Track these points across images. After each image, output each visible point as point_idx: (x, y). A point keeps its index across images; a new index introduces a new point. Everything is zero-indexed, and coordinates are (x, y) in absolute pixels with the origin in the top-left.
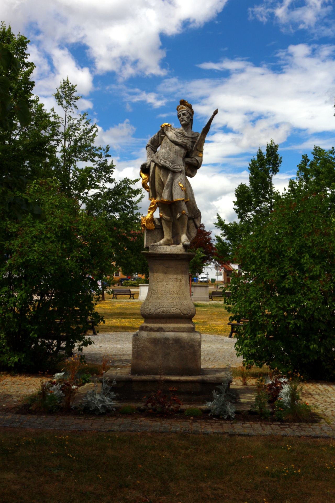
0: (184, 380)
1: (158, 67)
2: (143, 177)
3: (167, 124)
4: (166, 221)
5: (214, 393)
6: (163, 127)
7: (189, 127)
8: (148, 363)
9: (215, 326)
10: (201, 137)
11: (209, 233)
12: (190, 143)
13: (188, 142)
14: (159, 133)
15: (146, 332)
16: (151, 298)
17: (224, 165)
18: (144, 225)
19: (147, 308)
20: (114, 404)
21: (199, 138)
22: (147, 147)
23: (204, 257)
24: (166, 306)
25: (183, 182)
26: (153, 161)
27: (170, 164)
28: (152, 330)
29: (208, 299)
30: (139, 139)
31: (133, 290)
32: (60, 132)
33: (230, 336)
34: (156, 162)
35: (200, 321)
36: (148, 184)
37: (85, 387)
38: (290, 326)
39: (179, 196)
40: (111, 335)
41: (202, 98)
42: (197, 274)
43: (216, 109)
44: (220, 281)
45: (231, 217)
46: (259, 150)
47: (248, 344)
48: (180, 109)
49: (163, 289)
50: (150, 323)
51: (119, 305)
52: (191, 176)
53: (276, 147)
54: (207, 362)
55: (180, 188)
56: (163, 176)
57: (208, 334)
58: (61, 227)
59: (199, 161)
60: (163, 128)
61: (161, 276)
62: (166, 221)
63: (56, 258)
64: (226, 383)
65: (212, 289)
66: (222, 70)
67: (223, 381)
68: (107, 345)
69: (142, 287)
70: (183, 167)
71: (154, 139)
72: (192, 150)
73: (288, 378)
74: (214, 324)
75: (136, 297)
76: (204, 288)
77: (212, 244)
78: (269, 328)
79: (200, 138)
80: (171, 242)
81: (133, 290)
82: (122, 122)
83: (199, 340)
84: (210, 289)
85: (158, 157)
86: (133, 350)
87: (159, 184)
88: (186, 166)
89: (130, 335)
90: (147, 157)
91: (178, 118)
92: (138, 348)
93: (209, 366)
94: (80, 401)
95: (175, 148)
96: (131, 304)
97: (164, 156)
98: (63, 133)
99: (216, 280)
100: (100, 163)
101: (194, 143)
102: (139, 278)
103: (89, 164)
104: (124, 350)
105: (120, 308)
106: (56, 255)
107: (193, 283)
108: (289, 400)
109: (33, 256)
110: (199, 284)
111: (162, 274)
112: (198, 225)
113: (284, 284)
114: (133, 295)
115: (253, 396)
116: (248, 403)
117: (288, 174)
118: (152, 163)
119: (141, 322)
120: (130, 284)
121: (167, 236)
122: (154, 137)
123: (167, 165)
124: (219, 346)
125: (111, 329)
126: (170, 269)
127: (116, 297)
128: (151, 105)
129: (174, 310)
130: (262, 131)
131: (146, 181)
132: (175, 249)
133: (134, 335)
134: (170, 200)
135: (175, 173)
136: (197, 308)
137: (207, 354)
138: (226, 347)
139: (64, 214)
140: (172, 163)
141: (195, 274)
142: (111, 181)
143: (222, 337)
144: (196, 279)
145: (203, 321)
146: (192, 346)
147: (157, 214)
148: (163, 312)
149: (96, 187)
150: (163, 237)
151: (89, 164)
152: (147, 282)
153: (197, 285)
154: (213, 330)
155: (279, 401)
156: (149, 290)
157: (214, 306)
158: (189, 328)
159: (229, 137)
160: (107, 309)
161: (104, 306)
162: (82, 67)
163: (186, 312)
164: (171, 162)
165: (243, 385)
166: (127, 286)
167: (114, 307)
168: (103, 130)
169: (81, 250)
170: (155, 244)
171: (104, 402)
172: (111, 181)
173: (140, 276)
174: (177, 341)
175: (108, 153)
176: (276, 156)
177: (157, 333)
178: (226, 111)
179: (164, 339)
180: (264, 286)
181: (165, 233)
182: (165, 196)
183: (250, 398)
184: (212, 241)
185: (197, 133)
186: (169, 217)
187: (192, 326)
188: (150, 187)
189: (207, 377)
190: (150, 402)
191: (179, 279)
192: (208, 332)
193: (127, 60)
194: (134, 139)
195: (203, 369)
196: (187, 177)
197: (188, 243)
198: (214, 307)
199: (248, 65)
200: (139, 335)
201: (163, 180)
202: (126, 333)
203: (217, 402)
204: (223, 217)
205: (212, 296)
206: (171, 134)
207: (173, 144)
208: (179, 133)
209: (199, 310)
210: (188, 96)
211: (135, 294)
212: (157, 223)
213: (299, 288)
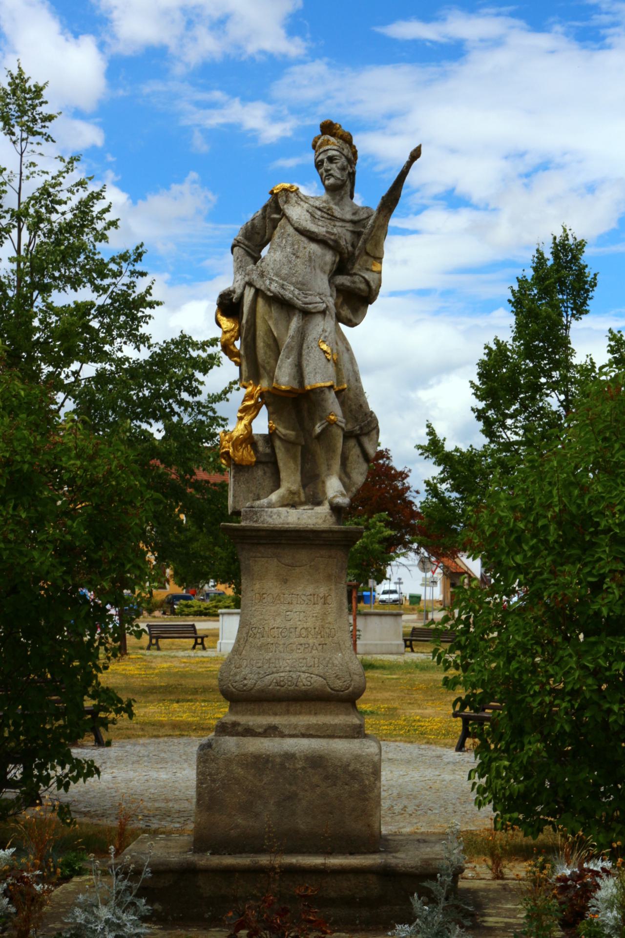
0: (334, 865)
1: (282, 32)
2: (224, 326)
3: (287, 185)
4: (285, 441)
5: (416, 902)
6: (277, 194)
7: (345, 193)
9: (419, 721)
10: (377, 218)
11: (403, 475)
12: (348, 236)
13: (343, 233)
16: (247, 648)
17: (447, 293)
18: (227, 453)
19: (235, 675)
20: (148, 931)
21: (371, 222)
22: (233, 247)
23: (391, 537)
24: (288, 668)
26: (250, 284)
27: (297, 292)
28: (249, 732)
29: (402, 648)
30: (223, 226)
31: (202, 625)
32: (5, 208)
33: (460, 747)
34: (258, 286)
35: (379, 708)
36: (238, 344)
37: (69, 886)
39: (319, 377)
40: (144, 747)
41: (390, 116)
42: (372, 583)
43: (417, 145)
44: (433, 601)
45: (464, 434)
46: (538, 250)
48: (320, 147)
49: (279, 622)
51: (165, 665)
52: (351, 324)
53: (580, 246)
54: (397, 818)
55: (322, 356)
56: (276, 324)
57: (401, 741)
59: (372, 284)
60: (275, 196)
61: (272, 587)
62: (285, 441)
64: (448, 875)
65: (411, 620)
66: (443, 40)
67: (438, 870)
68: (131, 774)
69: (226, 618)
70: (330, 299)
71: (253, 226)
72: (353, 254)
73: (613, 857)
74: (417, 714)
75: (211, 644)
76: (388, 621)
77: (411, 503)
78: (559, 725)
79: (375, 222)
80: (299, 497)
81: (202, 625)
82: (180, 181)
83: (376, 758)
84: (408, 621)
85: (263, 272)
86: (198, 787)
87: (268, 346)
88: (337, 297)
89: (191, 746)
90: (235, 273)
91: (315, 170)
92: (213, 781)
93: (404, 827)
94: (58, 925)
95: (308, 249)
96: (197, 663)
97: (280, 269)
98: (13, 210)
99: (423, 598)
101: (357, 234)
102: (219, 594)
103: (85, 294)
104: (177, 785)
105: (169, 674)
107: (361, 605)
108: (616, 918)
110: (376, 608)
112: (372, 453)
113: (595, 607)
114: (202, 638)
115: (520, 910)
116: (508, 926)
117: (616, 315)
118: (247, 288)
119: (221, 712)
120: (196, 609)
121: (290, 481)
122: (253, 220)
123: (288, 295)
124: (430, 773)
125: (143, 730)
126: (298, 570)
127: (157, 643)
128: (252, 136)
129: (308, 680)
130: (550, 201)
131: (232, 336)
132: (309, 517)
133: (202, 747)
134: (296, 386)
135: (307, 314)
136: (370, 674)
137: (398, 794)
138: (447, 777)
139: (17, 428)
140: (299, 289)
141: (367, 583)
142: (143, 340)
143: (439, 750)
144: (369, 596)
145: (388, 708)
146: (355, 776)
147: (261, 425)
148: (278, 684)
149: (103, 356)
150: (277, 486)
151: (85, 294)
152: (237, 605)
153: (372, 610)
154: (415, 730)
155: (591, 923)
156: (242, 625)
157: (417, 666)
158: (349, 726)
159: (463, 219)
160: (132, 676)
161: (124, 670)
162: (76, 36)
163: (338, 684)
165: (494, 879)
166: (188, 615)
167: (151, 671)
168: (130, 201)
170: (258, 503)
171: (120, 927)
173: (221, 587)
174: (316, 761)
176: (581, 273)
177: (262, 740)
178: (453, 151)
179: (280, 756)
180: (544, 613)
181: (283, 475)
182: (284, 377)
183: (512, 913)
184: (410, 496)
185: (367, 208)
187: (356, 721)
188: (242, 352)
189: (396, 858)
190: (243, 928)
191: (321, 595)
192: (401, 735)
193: (198, 15)
194: (211, 225)
195: (386, 835)
196: (341, 325)
197: (344, 501)
198: (418, 671)
199: (512, 27)
200: (214, 745)
201: (276, 335)
202: (183, 740)
203: (424, 926)
204: (440, 433)
205: (411, 641)
206: (296, 212)
207: (303, 239)
208: (319, 209)
209: (378, 678)
210: (354, 111)
211: (207, 636)
212: (261, 449)
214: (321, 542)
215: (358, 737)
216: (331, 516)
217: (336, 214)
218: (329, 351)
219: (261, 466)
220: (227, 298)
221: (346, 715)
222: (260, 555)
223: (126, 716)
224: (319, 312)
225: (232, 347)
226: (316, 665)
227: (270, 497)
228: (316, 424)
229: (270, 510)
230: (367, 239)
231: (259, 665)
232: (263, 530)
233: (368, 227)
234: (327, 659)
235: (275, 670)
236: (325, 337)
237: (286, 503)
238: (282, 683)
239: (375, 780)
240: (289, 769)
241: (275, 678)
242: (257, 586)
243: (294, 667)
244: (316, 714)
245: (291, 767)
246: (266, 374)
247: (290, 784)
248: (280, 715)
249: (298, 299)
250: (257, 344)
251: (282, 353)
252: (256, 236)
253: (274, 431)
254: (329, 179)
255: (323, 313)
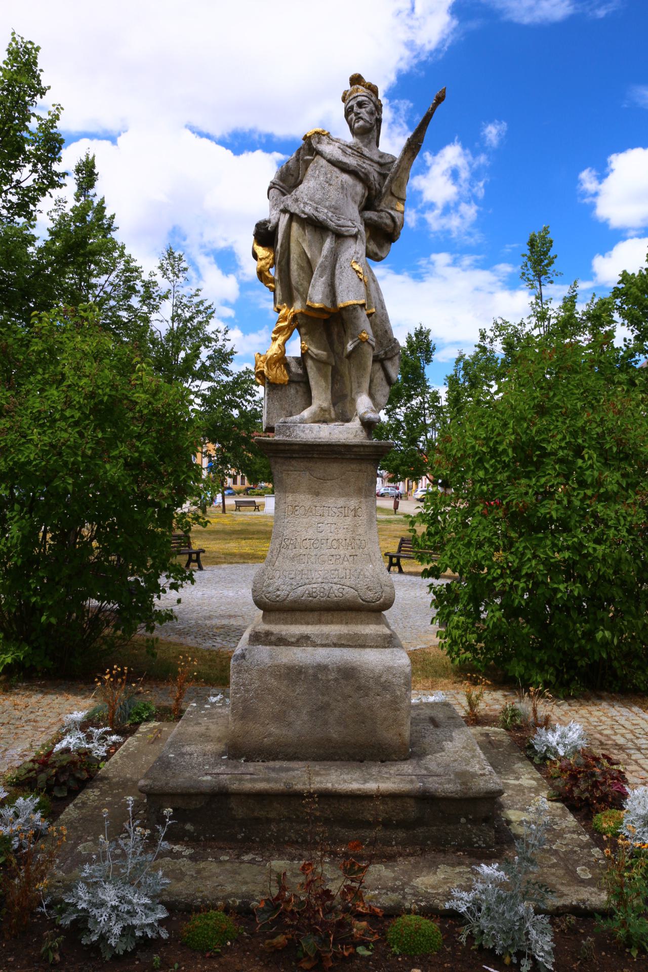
4: (317, 361)
8: (273, 729)
14: (298, 152)
15: (268, 647)
16: (280, 558)
19: (269, 586)
24: (320, 580)
25: (361, 260)
27: (330, 214)
28: (282, 641)
31: (258, 500)
34: (292, 211)
38: (559, 595)
39: (351, 295)
40: (224, 570)
47: (460, 624)
49: (310, 533)
50: (276, 624)
56: (310, 246)
58: (92, 395)
59: (397, 220)
62: (317, 361)
63: (80, 459)
71: (288, 168)
72: (380, 192)
80: (330, 414)
81: (258, 500)
87: (301, 268)
90: (271, 210)
95: (340, 179)
100: (217, 348)
101: (383, 176)
106: (80, 453)
109: (30, 454)
111: (309, 496)
118: (282, 215)
121: (321, 398)
123: (322, 217)
125: (225, 558)
126: (329, 483)
134: (328, 305)
135: (339, 236)
142: (227, 373)
148: (310, 595)
150: (309, 403)
158: (380, 636)
160: (226, 525)
163: (370, 595)
164: (332, 210)
169: (138, 444)
170: (290, 419)
172: (227, 373)
175: (227, 337)
176: (429, 343)
179: (313, 667)
181: (314, 393)
182: (317, 296)
186: (325, 353)
188: (276, 278)
191: (352, 508)
200: (247, 657)
201: (309, 256)
202: (244, 566)
207: (336, 169)
208: (350, 147)
212: (293, 369)
213: (577, 519)
214: (353, 456)
215: (388, 647)
216: (362, 431)
217: (365, 153)
218: (361, 271)
219: (293, 385)
220: (263, 227)
221: (377, 624)
222: (292, 468)
223: (189, 582)
224: (351, 236)
225: (267, 273)
226: (348, 577)
227: (302, 414)
228: (348, 342)
229: (303, 425)
230: (393, 178)
231: (292, 576)
232: (296, 444)
233: (393, 170)
234: (358, 571)
235: (307, 581)
236: (357, 258)
237: (317, 419)
238: (314, 595)
239: (407, 691)
240: (321, 680)
241: (307, 589)
242: (290, 498)
243: (326, 578)
244: (347, 623)
245: (324, 678)
246: (299, 296)
247: (323, 695)
248: (312, 624)
249: (331, 220)
250: (291, 268)
251: (315, 273)
252: (291, 177)
253: (307, 351)
254: (358, 122)
255: (355, 237)
